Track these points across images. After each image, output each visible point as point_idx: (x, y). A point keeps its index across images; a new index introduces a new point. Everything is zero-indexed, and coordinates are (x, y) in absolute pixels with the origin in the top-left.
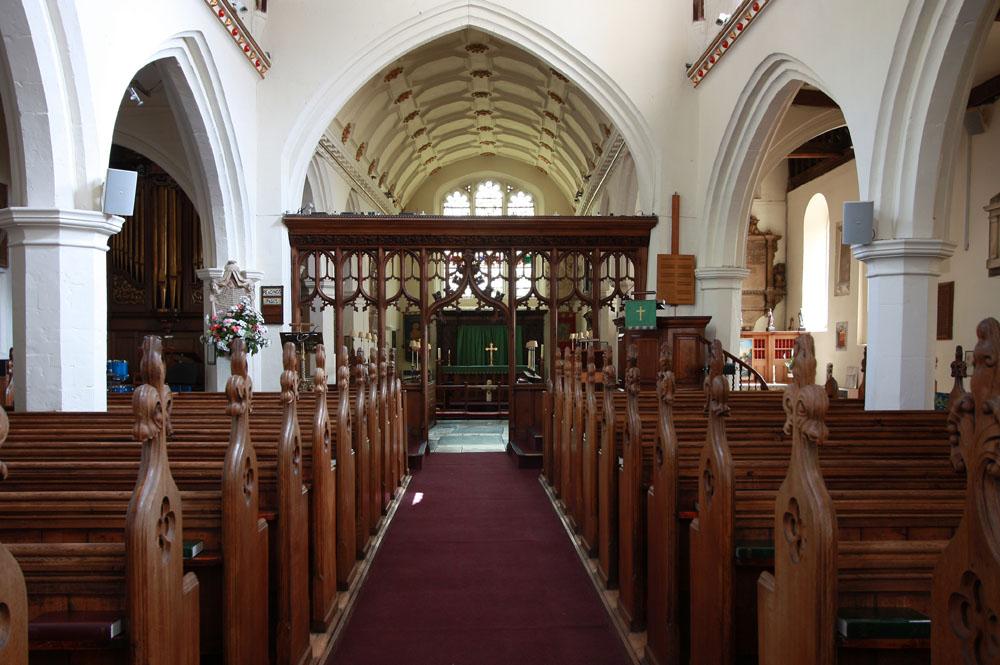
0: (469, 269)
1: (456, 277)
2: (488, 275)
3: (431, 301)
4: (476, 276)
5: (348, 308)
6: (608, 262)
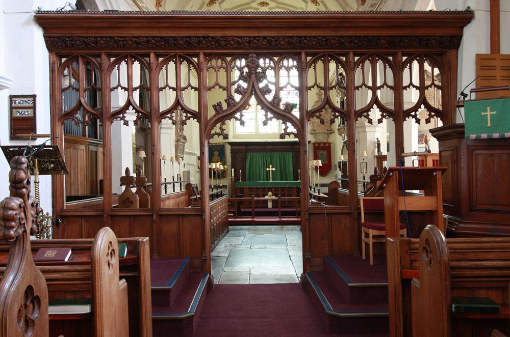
0: (253, 76)
1: (239, 86)
2: (277, 84)
3: (211, 113)
4: (261, 85)
5: (363, 120)
6: (410, 69)
